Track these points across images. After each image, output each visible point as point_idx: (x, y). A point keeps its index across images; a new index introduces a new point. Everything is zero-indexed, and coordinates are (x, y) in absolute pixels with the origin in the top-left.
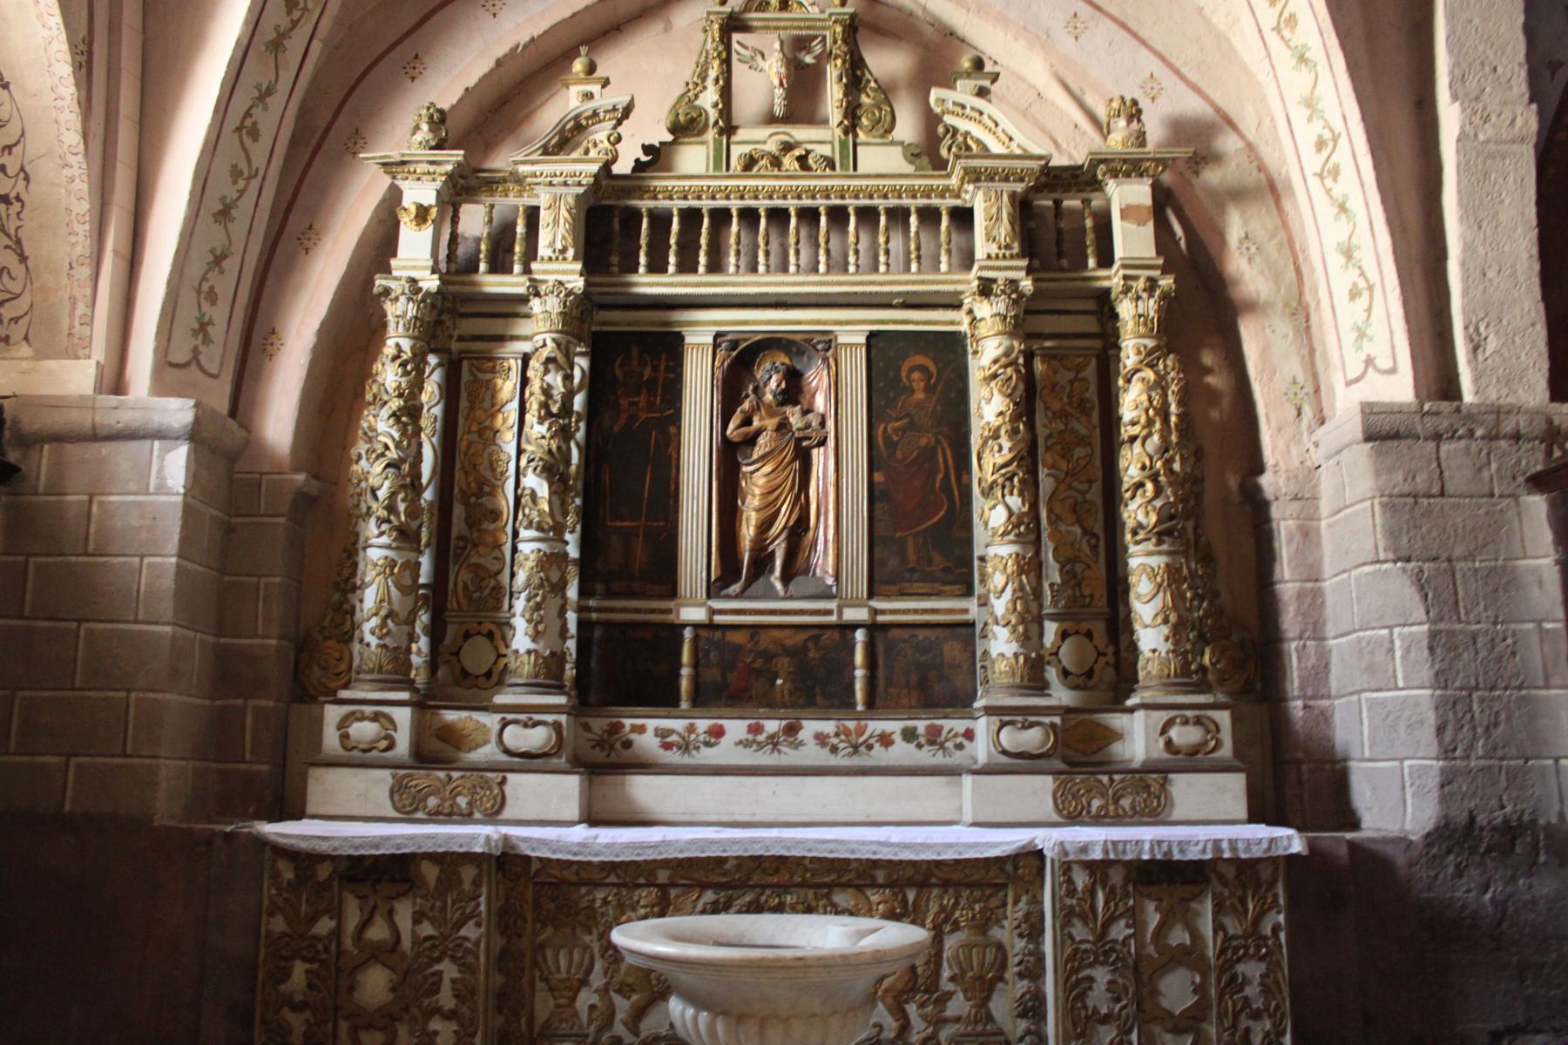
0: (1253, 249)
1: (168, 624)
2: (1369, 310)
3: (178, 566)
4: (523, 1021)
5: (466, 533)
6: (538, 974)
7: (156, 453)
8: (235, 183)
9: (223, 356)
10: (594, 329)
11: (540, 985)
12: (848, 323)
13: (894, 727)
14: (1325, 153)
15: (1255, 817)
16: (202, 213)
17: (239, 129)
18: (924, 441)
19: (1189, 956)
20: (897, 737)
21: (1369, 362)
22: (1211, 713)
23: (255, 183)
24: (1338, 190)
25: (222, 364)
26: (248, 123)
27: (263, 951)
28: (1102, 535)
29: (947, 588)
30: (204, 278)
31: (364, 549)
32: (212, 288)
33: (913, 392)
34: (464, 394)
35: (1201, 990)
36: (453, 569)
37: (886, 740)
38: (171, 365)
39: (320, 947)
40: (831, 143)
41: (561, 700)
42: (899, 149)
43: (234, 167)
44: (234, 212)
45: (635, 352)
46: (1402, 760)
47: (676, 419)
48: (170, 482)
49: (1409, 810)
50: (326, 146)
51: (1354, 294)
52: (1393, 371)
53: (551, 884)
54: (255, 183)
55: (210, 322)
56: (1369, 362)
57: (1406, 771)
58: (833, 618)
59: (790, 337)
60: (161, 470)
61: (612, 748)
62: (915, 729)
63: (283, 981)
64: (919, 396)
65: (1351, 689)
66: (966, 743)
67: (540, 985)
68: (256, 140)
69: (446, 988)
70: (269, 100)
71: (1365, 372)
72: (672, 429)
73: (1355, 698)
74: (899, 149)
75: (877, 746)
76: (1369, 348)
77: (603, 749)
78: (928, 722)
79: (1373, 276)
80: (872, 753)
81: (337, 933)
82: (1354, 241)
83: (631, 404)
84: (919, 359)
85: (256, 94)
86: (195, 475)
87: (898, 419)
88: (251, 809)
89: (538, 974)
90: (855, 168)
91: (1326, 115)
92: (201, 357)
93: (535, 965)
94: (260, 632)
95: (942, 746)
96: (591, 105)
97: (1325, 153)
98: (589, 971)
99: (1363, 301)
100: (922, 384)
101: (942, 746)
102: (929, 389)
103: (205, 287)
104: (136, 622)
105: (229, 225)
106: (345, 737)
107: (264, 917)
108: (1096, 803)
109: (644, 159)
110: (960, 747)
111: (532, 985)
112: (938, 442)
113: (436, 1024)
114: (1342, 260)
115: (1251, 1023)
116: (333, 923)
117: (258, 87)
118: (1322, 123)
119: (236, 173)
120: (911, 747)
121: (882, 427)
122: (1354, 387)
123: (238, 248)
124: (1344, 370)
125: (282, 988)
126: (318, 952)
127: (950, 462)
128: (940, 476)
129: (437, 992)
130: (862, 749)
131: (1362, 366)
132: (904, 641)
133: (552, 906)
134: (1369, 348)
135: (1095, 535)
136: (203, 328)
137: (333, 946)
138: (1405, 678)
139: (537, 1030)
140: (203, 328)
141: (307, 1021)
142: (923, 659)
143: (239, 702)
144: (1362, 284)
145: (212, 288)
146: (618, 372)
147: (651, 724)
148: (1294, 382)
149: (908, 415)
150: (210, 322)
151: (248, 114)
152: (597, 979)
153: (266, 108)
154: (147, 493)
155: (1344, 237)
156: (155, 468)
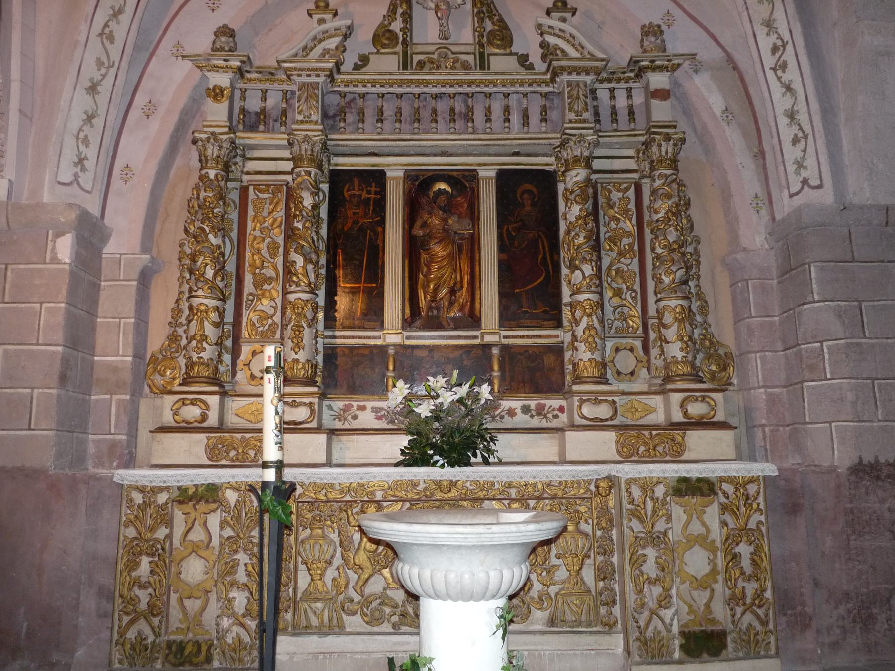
0: (731, 117)
1: (60, 346)
2: (805, 151)
3: (66, 309)
4: (291, 590)
5: (254, 291)
6: (300, 559)
7: (50, 237)
8: (99, 69)
9: (94, 180)
10: (331, 168)
11: (302, 567)
12: (485, 165)
13: (515, 404)
14: (777, 55)
15: (739, 458)
16: (77, 88)
17: (101, 35)
18: (531, 235)
19: (703, 541)
20: (518, 411)
21: (805, 182)
22: (711, 394)
23: (113, 71)
24: (786, 77)
25: (94, 185)
26: (107, 31)
27: (121, 551)
28: (639, 291)
29: (545, 323)
30: (80, 130)
31: (713, 621)
32: (86, 136)
33: (524, 206)
34: (250, 207)
35: (712, 562)
36: (245, 313)
37: (511, 412)
38: (59, 183)
39: (159, 546)
40: (474, 54)
41: (315, 389)
42: (515, 57)
43: (99, 59)
44: (99, 88)
45: (356, 182)
46: (830, 423)
47: (382, 222)
48: (60, 256)
49: (836, 452)
50: (158, 52)
51: (795, 141)
52: (820, 187)
53: (308, 502)
54: (113, 71)
55: (85, 158)
56: (805, 182)
57: (833, 429)
58: (477, 342)
59: (450, 174)
60: (54, 248)
61: (345, 419)
62: (529, 406)
63: (134, 570)
64: (528, 208)
65: (796, 381)
66: (559, 414)
67: (302, 567)
68: (112, 42)
69: (241, 570)
70: (120, 17)
71: (802, 188)
72: (380, 229)
73: (799, 385)
74: (515, 57)
75: (506, 416)
76: (804, 174)
77: (340, 420)
78: (537, 402)
79: (807, 129)
80: (503, 421)
81: (169, 537)
82: (795, 108)
83: (354, 213)
84: (528, 187)
85: (112, 12)
86: (76, 253)
87: (514, 223)
88: (115, 464)
89: (300, 559)
90: (489, 68)
91: (779, 31)
92: (79, 180)
93: (298, 553)
94: (121, 353)
95: (545, 416)
96: (324, 27)
97: (777, 55)
98: (332, 557)
99: (802, 144)
100: (529, 202)
101: (545, 416)
102: (533, 204)
103: (81, 135)
104: (38, 344)
105: (96, 96)
106: (685, 413)
107: (122, 528)
108: (642, 449)
109: (359, 63)
110: (556, 416)
111: (296, 567)
112: (539, 236)
113: (234, 594)
114: (786, 120)
115: (746, 584)
116: (167, 531)
117: (113, 8)
118: (776, 36)
119: (100, 63)
120: (527, 417)
121: (506, 227)
122: (795, 198)
123: (102, 111)
124: (788, 189)
125: (134, 574)
126: (157, 550)
127: (547, 248)
128: (541, 256)
129: (236, 572)
130: (498, 418)
131: (800, 185)
132: (521, 354)
133: (309, 516)
134: (804, 174)
135: (635, 291)
136: (80, 161)
137: (167, 544)
138: (832, 373)
139: (299, 595)
140: (80, 161)
141: (150, 594)
142: (533, 365)
143: (108, 396)
144: (800, 134)
145: (86, 136)
146: (346, 194)
147: (370, 404)
148: (756, 197)
149: (521, 220)
150: (85, 158)
151: (106, 25)
152: (338, 561)
153: (118, 23)
154: (45, 263)
155: (788, 106)
156: (49, 247)
